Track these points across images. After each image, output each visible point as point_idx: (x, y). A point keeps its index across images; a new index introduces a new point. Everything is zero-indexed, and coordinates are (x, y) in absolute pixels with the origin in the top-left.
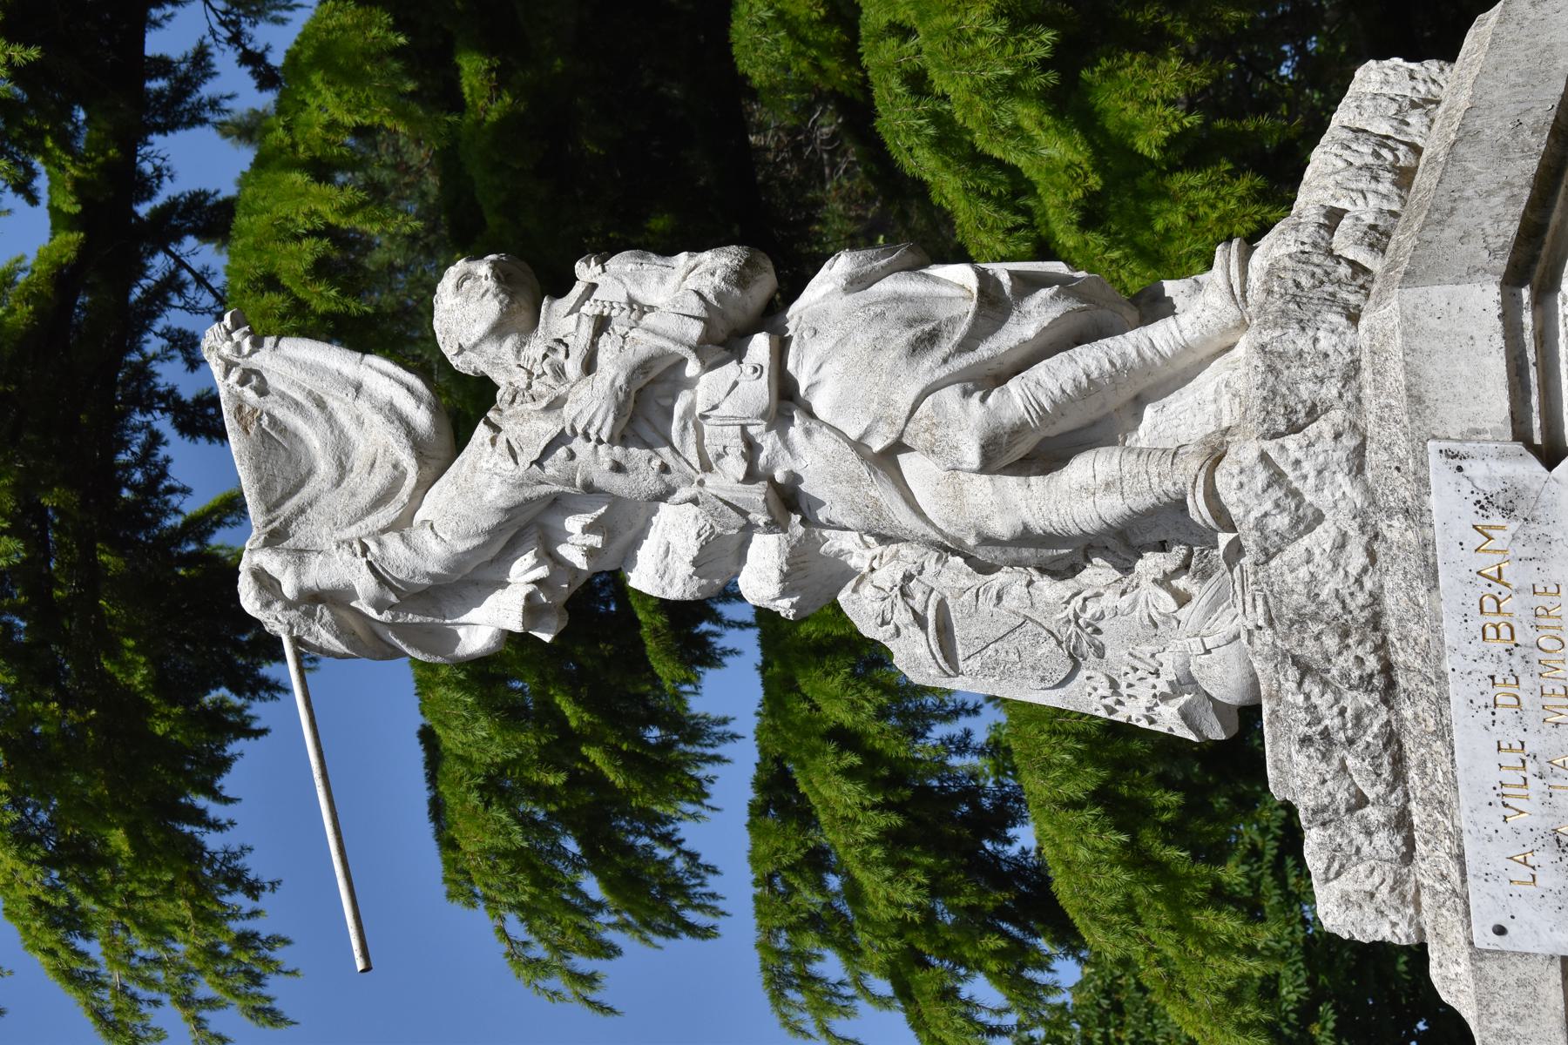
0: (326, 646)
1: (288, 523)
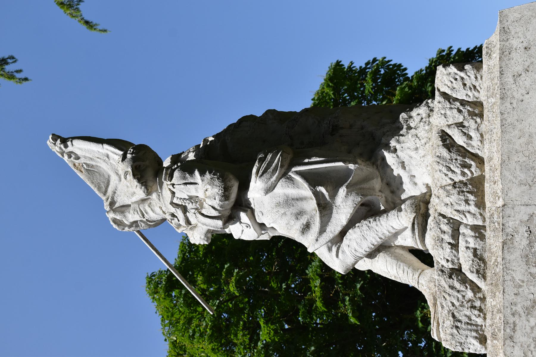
1: (113, 198)
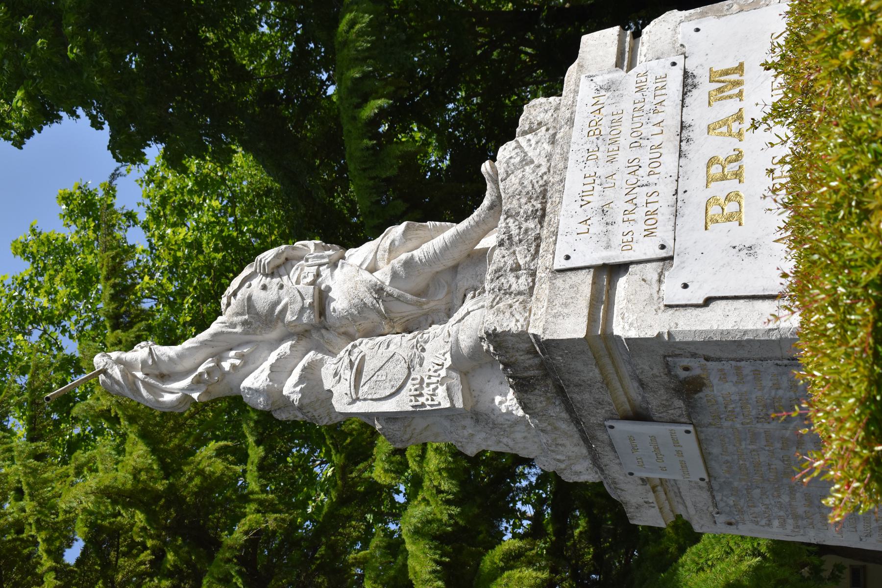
0: (114, 375)
